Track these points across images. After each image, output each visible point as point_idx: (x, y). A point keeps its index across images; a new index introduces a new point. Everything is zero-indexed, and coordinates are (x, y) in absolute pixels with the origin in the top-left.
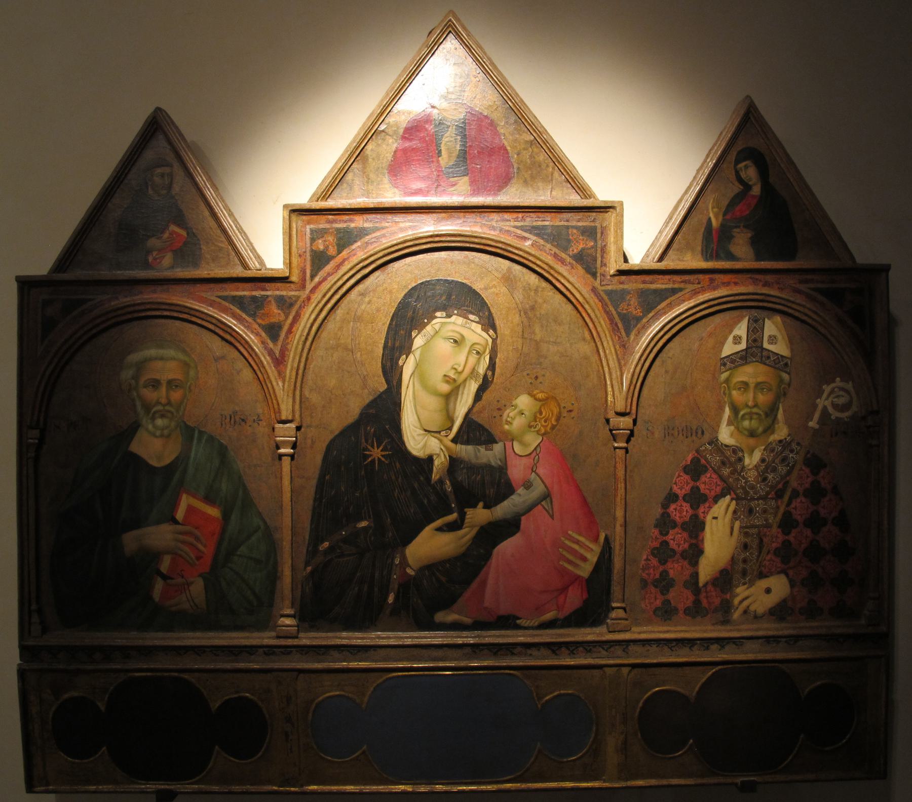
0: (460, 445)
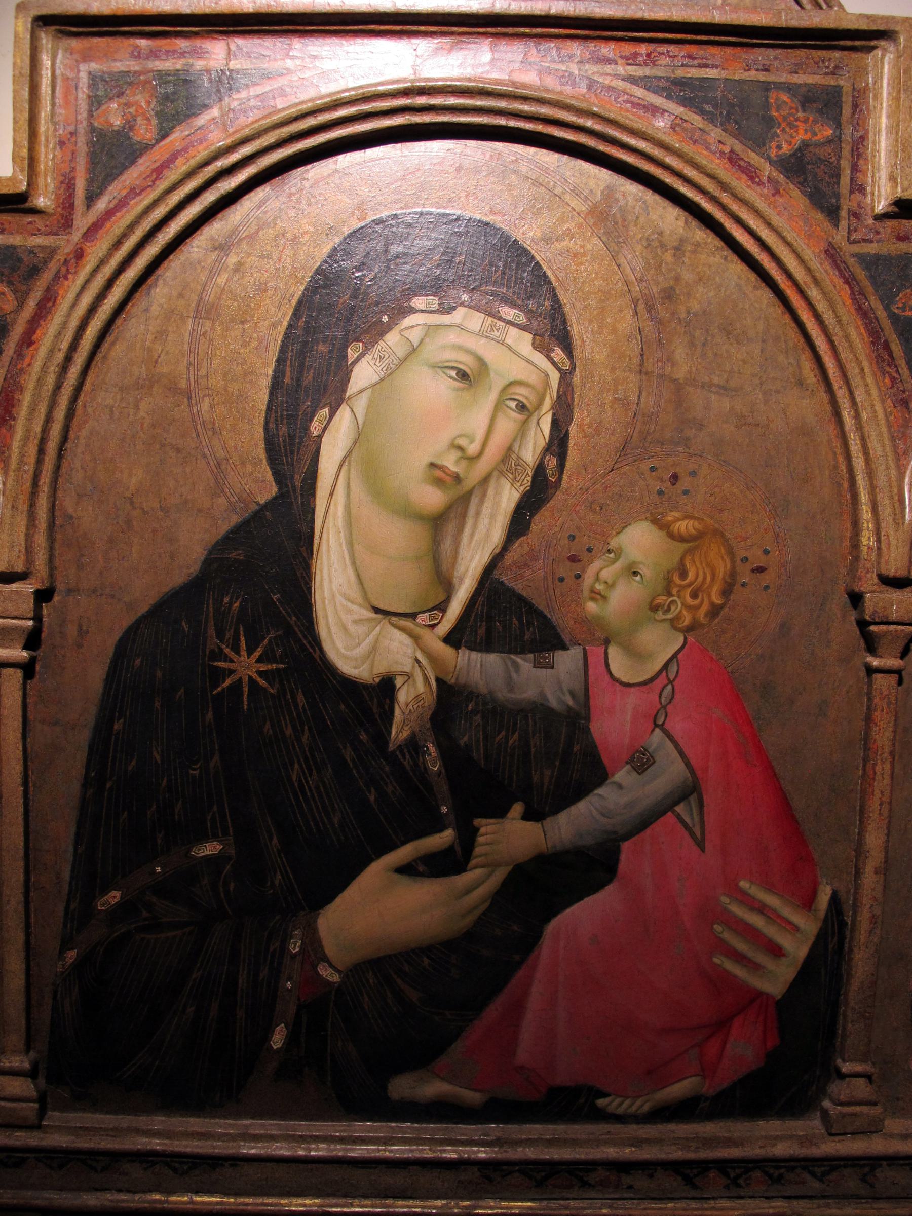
0: (467, 651)
